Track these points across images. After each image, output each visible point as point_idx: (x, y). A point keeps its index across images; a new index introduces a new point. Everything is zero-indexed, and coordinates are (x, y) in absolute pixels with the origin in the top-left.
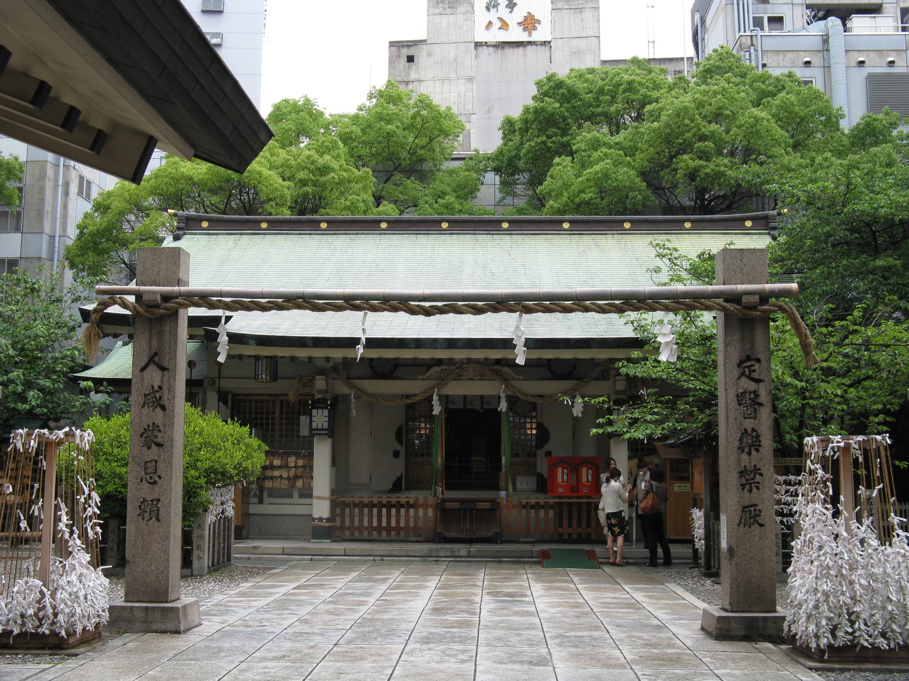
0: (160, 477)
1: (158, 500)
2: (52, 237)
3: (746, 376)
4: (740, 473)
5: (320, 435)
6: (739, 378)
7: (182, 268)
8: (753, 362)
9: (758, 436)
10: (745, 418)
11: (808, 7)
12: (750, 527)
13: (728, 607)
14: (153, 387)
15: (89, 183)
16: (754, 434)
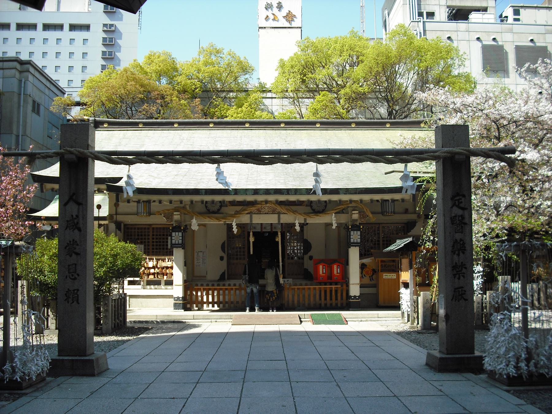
0: (78, 275)
1: (78, 290)
2: (18, 136)
3: (457, 206)
4: (453, 267)
5: (177, 247)
6: (452, 207)
7: (90, 138)
8: (461, 197)
9: (464, 244)
10: (456, 233)
11: (448, 7)
12: (459, 301)
13: (445, 352)
14: (72, 216)
15: (39, 105)
16: (462, 242)
